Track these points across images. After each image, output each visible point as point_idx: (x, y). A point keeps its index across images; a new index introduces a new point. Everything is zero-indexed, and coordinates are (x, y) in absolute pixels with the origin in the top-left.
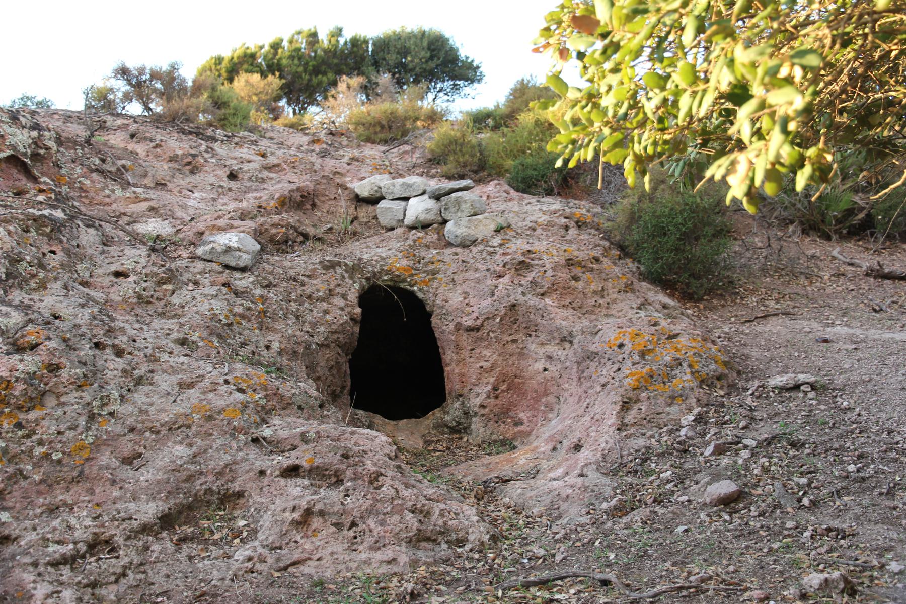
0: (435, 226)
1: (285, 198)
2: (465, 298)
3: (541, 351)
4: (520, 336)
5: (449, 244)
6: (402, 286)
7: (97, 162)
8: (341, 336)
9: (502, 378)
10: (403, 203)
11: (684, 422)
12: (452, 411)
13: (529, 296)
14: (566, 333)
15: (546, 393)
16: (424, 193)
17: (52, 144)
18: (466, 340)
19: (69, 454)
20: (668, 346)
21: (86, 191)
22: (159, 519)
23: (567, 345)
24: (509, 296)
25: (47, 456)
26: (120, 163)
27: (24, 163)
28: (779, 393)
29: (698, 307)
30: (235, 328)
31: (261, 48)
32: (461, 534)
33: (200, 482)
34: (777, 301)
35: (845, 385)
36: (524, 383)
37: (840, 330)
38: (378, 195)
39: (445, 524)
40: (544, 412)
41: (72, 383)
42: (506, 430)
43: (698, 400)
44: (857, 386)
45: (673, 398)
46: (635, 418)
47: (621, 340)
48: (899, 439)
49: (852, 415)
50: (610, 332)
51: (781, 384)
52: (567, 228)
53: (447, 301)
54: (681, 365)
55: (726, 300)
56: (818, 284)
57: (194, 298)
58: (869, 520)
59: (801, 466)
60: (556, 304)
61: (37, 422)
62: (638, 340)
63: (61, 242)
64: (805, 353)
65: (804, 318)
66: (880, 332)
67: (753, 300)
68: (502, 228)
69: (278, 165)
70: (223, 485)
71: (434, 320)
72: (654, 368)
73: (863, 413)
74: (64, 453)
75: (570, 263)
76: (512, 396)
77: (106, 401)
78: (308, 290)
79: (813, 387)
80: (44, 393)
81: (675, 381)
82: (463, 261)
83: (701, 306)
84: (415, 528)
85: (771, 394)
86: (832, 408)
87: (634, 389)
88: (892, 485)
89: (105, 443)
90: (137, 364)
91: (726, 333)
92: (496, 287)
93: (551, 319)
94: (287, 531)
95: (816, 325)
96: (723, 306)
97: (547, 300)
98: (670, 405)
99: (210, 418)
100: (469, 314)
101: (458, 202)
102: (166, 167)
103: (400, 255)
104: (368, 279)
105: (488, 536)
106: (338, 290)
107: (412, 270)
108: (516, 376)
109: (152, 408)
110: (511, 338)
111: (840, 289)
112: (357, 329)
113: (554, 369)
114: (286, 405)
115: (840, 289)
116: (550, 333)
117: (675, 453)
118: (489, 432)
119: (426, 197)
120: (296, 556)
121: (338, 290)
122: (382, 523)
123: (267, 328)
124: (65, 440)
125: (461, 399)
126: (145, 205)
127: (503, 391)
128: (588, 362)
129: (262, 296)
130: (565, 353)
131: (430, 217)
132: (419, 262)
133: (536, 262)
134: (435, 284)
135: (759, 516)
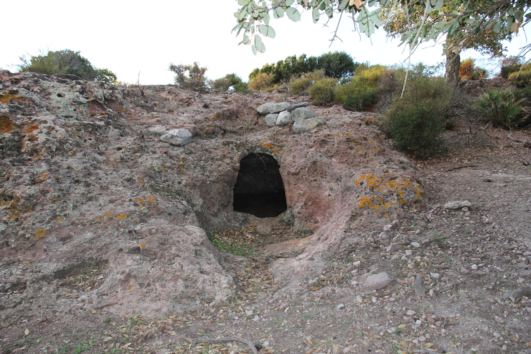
1: (220, 114)
3: (328, 185)
4: (318, 178)
5: (295, 133)
6: (267, 153)
7: (143, 102)
8: (226, 178)
9: (309, 199)
10: (277, 115)
11: (385, 229)
12: (286, 216)
13: (324, 157)
14: (338, 176)
15: (329, 208)
16: (285, 110)
17: (120, 96)
18: (292, 179)
19: (34, 235)
20: (387, 184)
21: (131, 114)
22: (55, 273)
23: (339, 183)
24: (313, 158)
25: (24, 235)
26: (154, 102)
27: (100, 103)
28: (449, 211)
29: (424, 163)
30: (163, 174)
31: (274, 65)
32: (212, 295)
33: (88, 253)
34: (469, 160)
35: (491, 208)
37: (500, 175)
38: (267, 112)
39: (203, 288)
40: (328, 217)
41: (51, 200)
42: (310, 225)
43: (399, 215)
44: (498, 209)
45: (383, 214)
46: (356, 225)
47: (362, 180)
48: (515, 246)
49: (488, 228)
50: (358, 176)
51: (450, 206)
52: (360, 125)
53: (285, 160)
54: (393, 195)
55: (440, 160)
56: (496, 151)
57: (147, 159)
58: (471, 312)
59: (441, 263)
61: (25, 218)
62: (371, 180)
63: (96, 134)
64: (475, 188)
65: (481, 169)
66: (523, 176)
67: (455, 160)
68: (321, 124)
69: (230, 101)
70: (99, 256)
71: (280, 169)
72: (375, 196)
73: (496, 226)
74: (32, 234)
75: (348, 140)
77: (65, 208)
78: (212, 155)
79: (469, 209)
80: (36, 204)
81: (387, 203)
83: (426, 163)
84: (180, 290)
85: (444, 212)
86: (477, 223)
87: (360, 208)
88: (498, 283)
89: (56, 230)
90: (94, 190)
91: (434, 177)
94: (115, 285)
95: (487, 172)
96: (438, 162)
97: (333, 159)
98: (380, 218)
99: (111, 219)
100: (294, 167)
101: (299, 113)
102: (175, 104)
103: (267, 138)
104: (248, 150)
105: (226, 298)
106: (228, 155)
107: (271, 146)
108: (316, 198)
109: (89, 213)
110: (313, 179)
111: (508, 154)
112: (237, 174)
114: (160, 213)
115: (508, 154)
116: (332, 176)
117: (371, 248)
118: (301, 226)
119: (286, 111)
120: (111, 301)
121: (228, 155)
122: (163, 286)
123: (183, 173)
124: (34, 227)
126: (155, 119)
127: (310, 205)
129: (183, 158)
131: (287, 120)
134: (281, 152)
135: (395, 301)
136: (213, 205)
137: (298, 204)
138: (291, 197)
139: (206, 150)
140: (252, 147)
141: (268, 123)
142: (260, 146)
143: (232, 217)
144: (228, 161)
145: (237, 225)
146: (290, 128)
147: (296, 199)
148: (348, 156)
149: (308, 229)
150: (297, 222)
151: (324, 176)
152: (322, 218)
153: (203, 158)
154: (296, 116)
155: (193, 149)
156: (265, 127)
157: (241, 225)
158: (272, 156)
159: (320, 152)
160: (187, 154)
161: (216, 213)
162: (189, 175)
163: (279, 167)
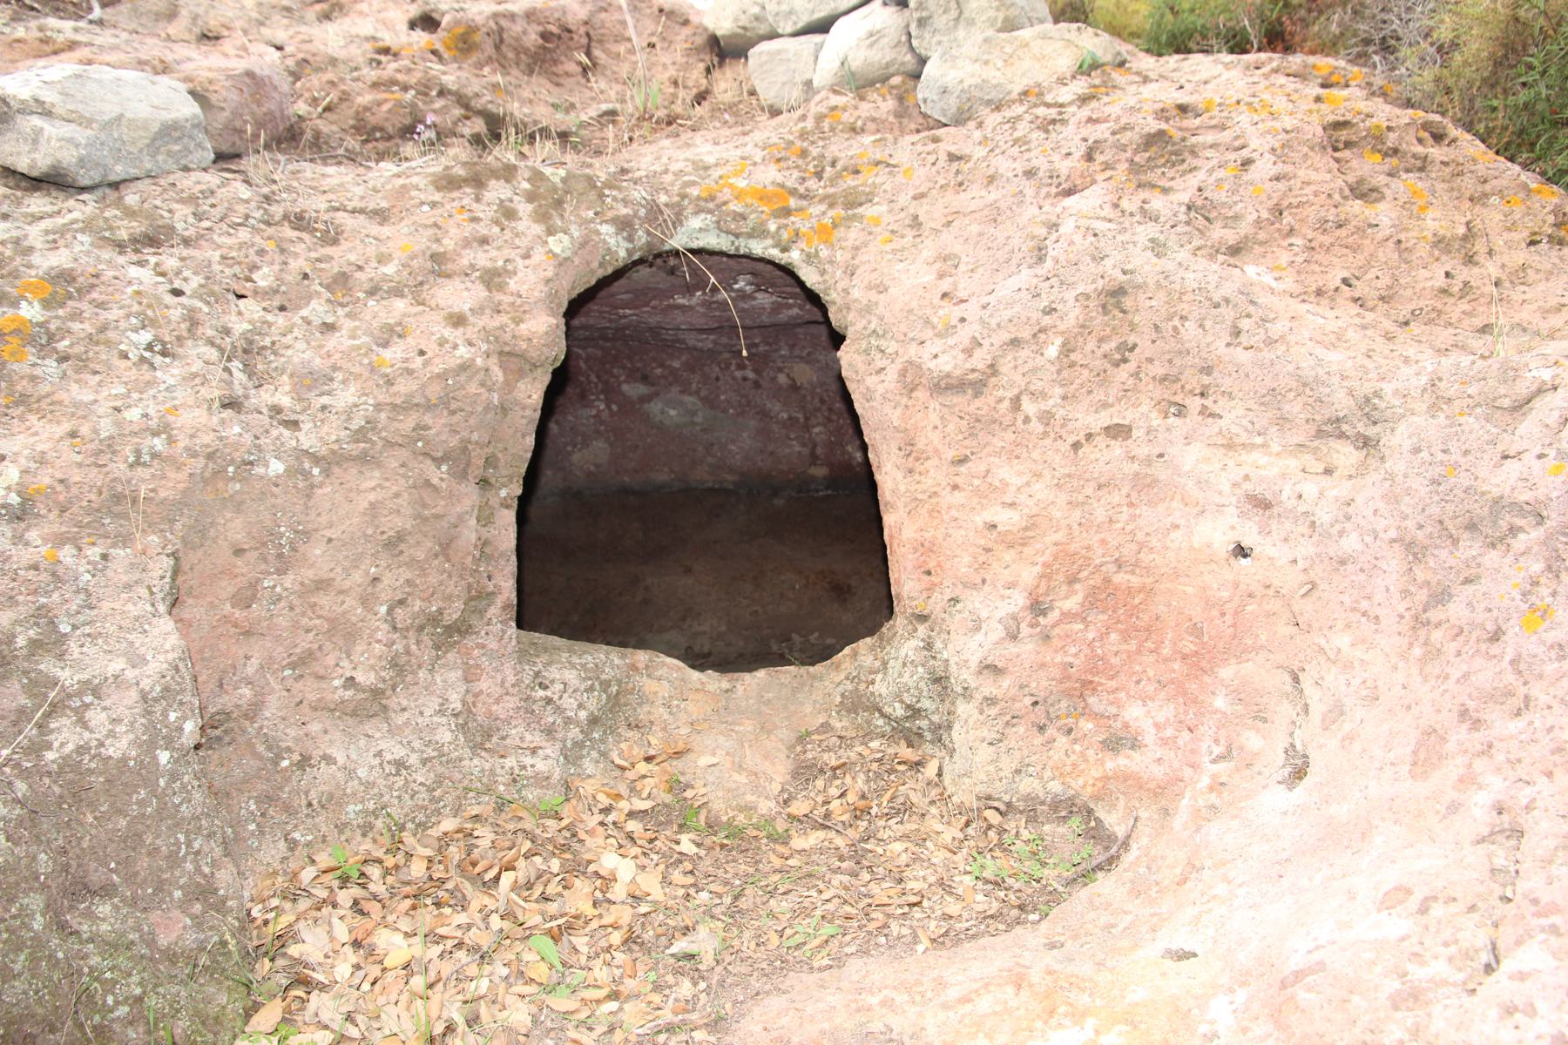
0: (896, 80)
2: (941, 276)
6: (758, 248)
8: (437, 423)
9: (1067, 567)
12: (885, 666)
14: (1342, 403)
18: (934, 422)
23: (1345, 455)
24: (1099, 258)
36: (1149, 592)
38: (763, 29)
53: (882, 289)
60: (1288, 283)
76: (1103, 637)
78: (342, 256)
82: (953, 158)
92: (1054, 226)
93: (1270, 342)
97: (1251, 270)
100: (949, 330)
107: (783, 204)
113: (1282, 554)
118: (1008, 765)
125: (922, 630)
127: (1068, 616)
128: (1470, 547)
130: (1338, 489)
131: (881, 55)
132: (819, 175)
133: (1210, 138)
134: (854, 234)
136: (345, 633)
137: (974, 601)
138: (926, 548)
139: (299, 221)
140: (654, 211)
141: (767, 94)
142: (706, 205)
143: (511, 703)
144: (459, 295)
145: (547, 762)
146: (901, 99)
147: (963, 565)
148: (1355, 249)
149: (1055, 787)
150: (969, 727)
151: (1195, 404)
152: (1166, 712)
153: (263, 278)
154: (940, 21)
155: (182, 211)
156: (749, 109)
157: (571, 755)
158: (788, 271)
159: (1148, 216)
160: (120, 247)
161: (377, 693)
162: (83, 410)
163: (837, 339)
